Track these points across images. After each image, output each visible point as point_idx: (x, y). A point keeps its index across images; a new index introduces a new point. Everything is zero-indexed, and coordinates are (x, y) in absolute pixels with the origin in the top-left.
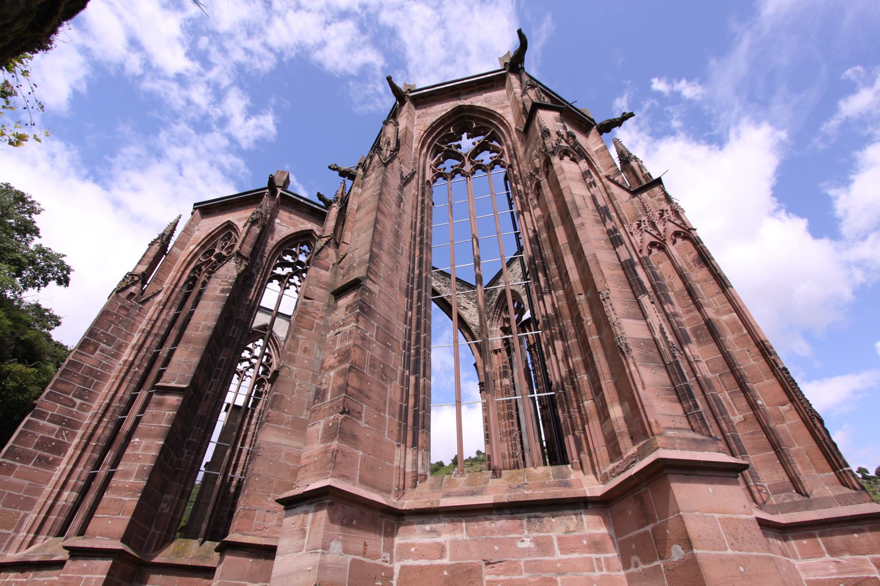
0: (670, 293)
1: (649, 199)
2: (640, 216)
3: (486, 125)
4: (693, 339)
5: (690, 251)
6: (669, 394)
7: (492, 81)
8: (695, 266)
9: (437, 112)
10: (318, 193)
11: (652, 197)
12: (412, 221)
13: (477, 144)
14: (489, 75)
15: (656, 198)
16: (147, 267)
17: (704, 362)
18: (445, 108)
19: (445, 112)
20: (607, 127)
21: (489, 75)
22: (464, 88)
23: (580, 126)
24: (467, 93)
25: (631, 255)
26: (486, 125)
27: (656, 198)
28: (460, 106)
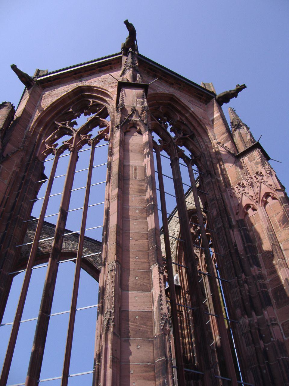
0: (259, 255)
1: (249, 162)
2: (241, 179)
3: (101, 103)
4: (274, 301)
5: (277, 212)
6: (146, 371)
7: (110, 64)
8: (281, 227)
9: (58, 94)
10: (92, 135)
11: (251, 161)
12: (4, 197)
13: (90, 119)
14: (107, 59)
15: (255, 161)
16: (117, 189)
17: (280, 324)
18: (67, 89)
19: (65, 93)
20: (226, 98)
21: (107, 59)
22: (85, 71)
23: (200, 98)
24: (88, 75)
25: (106, 238)
26: (101, 103)
27: (255, 161)
28: (80, 87)
